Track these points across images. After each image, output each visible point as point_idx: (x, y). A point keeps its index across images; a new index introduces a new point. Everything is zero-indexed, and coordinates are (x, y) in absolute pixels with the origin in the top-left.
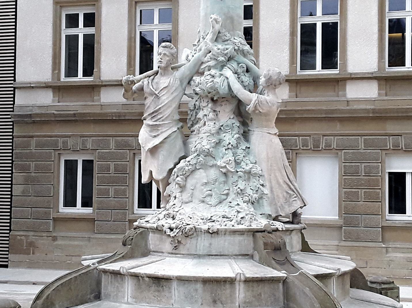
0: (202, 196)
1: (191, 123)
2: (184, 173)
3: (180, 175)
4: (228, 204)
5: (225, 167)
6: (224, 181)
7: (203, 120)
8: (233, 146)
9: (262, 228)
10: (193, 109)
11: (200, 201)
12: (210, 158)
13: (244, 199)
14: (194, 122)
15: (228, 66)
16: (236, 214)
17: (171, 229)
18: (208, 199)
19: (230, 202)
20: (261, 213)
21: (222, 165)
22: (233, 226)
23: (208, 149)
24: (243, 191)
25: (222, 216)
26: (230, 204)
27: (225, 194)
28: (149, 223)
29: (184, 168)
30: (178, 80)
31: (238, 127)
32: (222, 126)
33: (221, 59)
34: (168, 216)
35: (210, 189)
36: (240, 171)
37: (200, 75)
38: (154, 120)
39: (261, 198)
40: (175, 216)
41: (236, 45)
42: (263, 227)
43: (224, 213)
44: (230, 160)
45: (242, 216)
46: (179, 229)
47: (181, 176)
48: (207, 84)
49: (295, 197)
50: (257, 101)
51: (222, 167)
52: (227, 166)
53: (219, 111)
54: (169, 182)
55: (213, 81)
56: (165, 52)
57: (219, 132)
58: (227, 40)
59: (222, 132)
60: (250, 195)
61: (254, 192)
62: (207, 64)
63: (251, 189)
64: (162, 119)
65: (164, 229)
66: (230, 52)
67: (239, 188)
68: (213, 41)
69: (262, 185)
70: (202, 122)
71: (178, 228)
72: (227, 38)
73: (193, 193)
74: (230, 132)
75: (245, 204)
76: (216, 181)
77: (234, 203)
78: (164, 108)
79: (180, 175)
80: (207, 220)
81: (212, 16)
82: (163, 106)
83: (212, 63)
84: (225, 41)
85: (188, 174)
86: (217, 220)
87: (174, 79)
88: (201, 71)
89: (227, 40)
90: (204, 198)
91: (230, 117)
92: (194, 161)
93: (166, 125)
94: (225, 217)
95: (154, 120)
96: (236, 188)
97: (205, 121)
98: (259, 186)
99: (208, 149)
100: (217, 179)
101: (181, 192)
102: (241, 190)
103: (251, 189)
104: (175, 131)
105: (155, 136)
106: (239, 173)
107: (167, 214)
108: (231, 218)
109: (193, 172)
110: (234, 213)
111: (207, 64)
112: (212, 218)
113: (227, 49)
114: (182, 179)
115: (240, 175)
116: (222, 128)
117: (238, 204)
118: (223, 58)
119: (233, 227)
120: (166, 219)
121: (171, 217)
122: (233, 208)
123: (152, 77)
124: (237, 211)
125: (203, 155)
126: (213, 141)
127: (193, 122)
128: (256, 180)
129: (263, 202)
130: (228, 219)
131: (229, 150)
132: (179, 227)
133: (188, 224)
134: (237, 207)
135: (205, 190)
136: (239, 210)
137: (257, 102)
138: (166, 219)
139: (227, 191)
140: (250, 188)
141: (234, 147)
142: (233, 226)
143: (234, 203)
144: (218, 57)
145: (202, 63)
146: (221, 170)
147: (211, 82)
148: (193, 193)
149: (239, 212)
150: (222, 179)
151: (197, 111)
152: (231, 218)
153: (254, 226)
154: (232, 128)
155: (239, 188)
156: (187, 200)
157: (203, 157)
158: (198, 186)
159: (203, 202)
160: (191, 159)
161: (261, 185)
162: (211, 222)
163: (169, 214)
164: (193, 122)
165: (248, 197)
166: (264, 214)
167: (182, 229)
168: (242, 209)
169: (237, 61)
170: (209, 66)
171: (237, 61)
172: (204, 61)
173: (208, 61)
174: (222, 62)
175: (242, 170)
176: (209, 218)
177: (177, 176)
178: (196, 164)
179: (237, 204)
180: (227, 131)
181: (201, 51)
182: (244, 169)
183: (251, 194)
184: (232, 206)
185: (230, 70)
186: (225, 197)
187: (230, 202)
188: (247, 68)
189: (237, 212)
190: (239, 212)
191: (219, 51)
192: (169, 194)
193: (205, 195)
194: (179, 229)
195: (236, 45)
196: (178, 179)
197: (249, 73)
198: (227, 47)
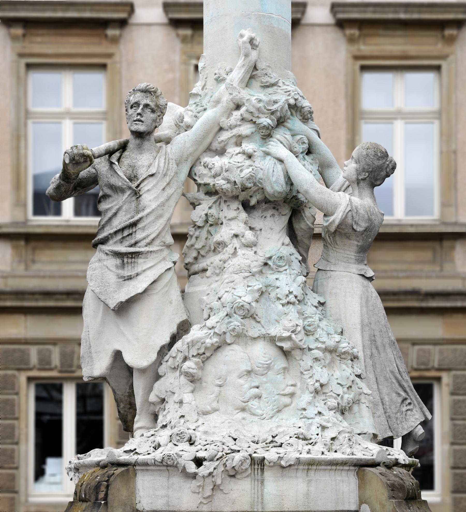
0: (241, 399)
1: (194, 254)
2: (201, 351)
3: (193, 356)
4: (300, 412)
5: (289, 338)
6: (285, 369)
7: (232, 245)
8: (298, 298)
9: (373, 459)
10: (201, 225)
11: (237, 409)
12: (253, 322)
13: (329, 403)
14: (202, 253)
15: (278, 136)
16: (319, 431)
17: (199, 462)
18: (254, 404)
19: (305, 409)
20: (359, 432)
21: (283, 335)
22: (323, 453)
23: (249, 304)
24: (324, 387)
25: (295, 436)
26: (304, 412)
27: (287, 395)
28: (137, 453)
29: (202, 341)
30: (174, 161)
31: (299, 262)
32: (270, 258)
33: (265, 121)
34: (178, 438)
35: (256, 384)
36: (317, 348)
37: (213, 154)
38: (127, 243)
39: (357, 402)
40: (193, 439)
41: (289, 95)
42: (374, 457)
43: (297, 431)
44: (297, 325)
45: (333, 436)
46: (218, 459)
47: (194, 359)
48: (241, 171)
49: (410, 404)
50: (349, 206)
51: (282, 339)
52: (293, 336)
53: (261, 230)
54: (160, 374)
55: (251, 166)
56: (148, 102)
57: (264, 271)
58: (272, 85)
59: (271, 272)
60: (339, 395)
61: (345, 389)
62: (235, 131)
63: (339, 384)
64: (144, 241)
65: (182, 462)
66: (282, 108)
67: (317, 381)
68: (244, 85)
69: (359, 376)
70: (229, 249)
71: (215, 459)
72: (273, 81)
73: (220, 391)
74: (286, 270)
75: (332, 412)
76: (269, 367)
77: (311, 412)
78: (151, 218)
79: (193, 356)
80: (266, 444)
81: (243, 32)
82: (148, 215)
83: (246, 129)
84: (268, 87)
85: (208, 354)
86: (288, 442)
87: (165, 159)
88: (216, 145)
89: (272, 85)
90: (245, 402)
91: (283, 241)
92: (222, 327)
93: (154, 255)
94: (301, 437)
95: (127, 243)
96: (311, 381)
97: (236, 248)
98: (353, 377)
99: (249, 304)
100: (271, 363)
101: (192, 392)
102: (322, 385)
103: (339, 384)
104: (169, 269)
105: (130, 278)
106: (313, 351)
107: (177, 434)
108: (311, 439)
109: (218, 348)
110: (314, 430)
111: (235, 131)
112: (276, 439)
113: (275, 102)
114: (197, 364)
115: (317, 356)
116: (270, 263)
117: (320, 413)
118: (269, 121)
119: (323, 456)
120: (175, 445)
121: (185, 440)
122: (310, 421)
123: (117, 154)
124: (321, 425)
125: (240, 316)
126: (256, 288)
127: (199, 252)
128: (348, 367)
129: (360, 409)
130: (306, 442)
131: (291, 306)
132: (217, 457)
133: (234, 451)
134: (318, 419)
135: (246, 386)
136: (324, 424)
137: (349, 208)
138: (175, 445)
139: (292, 388)
140: (336, 381)
141: (298, 300)
142: (323, 453)
143: (311, 412)
144: (258, 117)
145: (221, 129)
146: (279, 344)
147: (248, 168)
148: (220, 391)
149: (324, 428)
150: (281, 363)
151: (210, 228)
152: (311, 439)
153: (359, 455)
154: (289, 263)
155: (317, 381)
156: (209, 408)
157: (239, 318)
158: (233, 378)
159: (243, 410)
160: (217, 322)
161: (356, 376)
162: (275, 447)
163: (181, 433)
164: (199, 252)
165: (335, 398)
166: (365, 434)
167: (225, 460)
168: (328, 422)
169: (290, 130)
170: (239, 136)
171: (290, 130)
172: (225, 126)
173: (236, 126)
174: (266, 128)
175: (320, 345)
176: (270, 439)
177: (185, 359)
178: (225, 333)
179: (316, 412)
180: (281, 269)
181: (220, 106)
182: (324, 343)
183: (341, 393)
184: (308, 416)
185: (281, 145)
186: (287, 400)
187: (305, 409)
188: (309, 144)
189: (320, 428)
190: (324, 428)
191: (261, 105)
192: (163, 397)
193: (248, 395)
194: (218, 459)
195: (289, 95)
196: (188, 364)
197: (311, 156)
198: (274, 98)
